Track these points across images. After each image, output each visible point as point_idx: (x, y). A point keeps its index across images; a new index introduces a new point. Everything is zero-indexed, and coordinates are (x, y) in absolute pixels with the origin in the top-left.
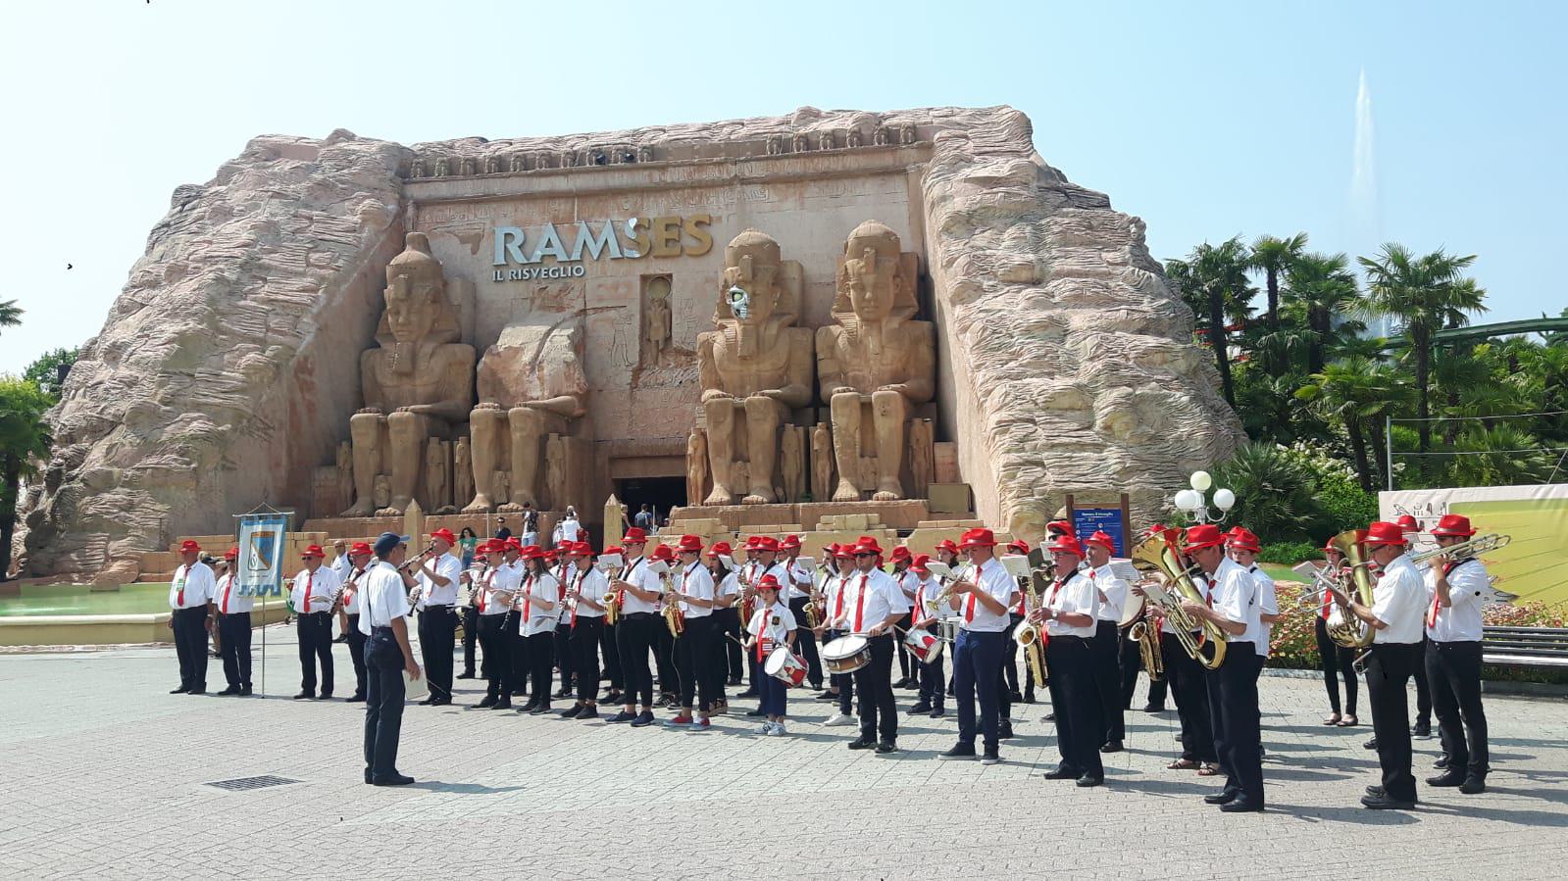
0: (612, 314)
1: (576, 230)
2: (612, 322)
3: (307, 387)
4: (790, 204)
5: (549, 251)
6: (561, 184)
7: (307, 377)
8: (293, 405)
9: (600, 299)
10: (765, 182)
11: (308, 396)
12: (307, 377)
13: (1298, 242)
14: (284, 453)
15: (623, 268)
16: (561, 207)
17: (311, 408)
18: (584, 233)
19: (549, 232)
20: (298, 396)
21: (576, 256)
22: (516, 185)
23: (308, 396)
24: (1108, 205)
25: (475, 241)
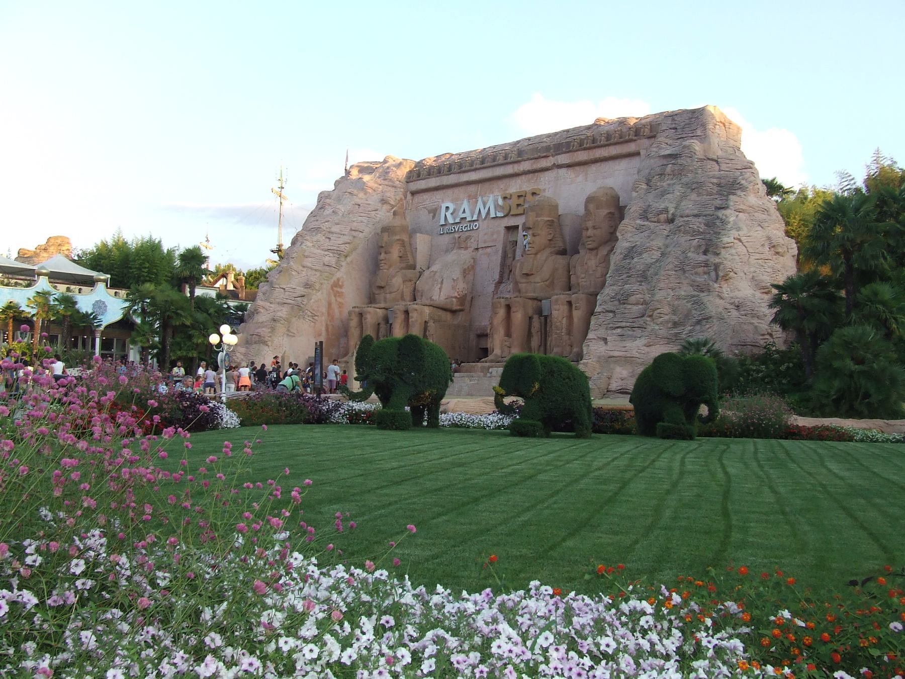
0: (489, 250)
1: (477, 202)
2: (489, 255)
3: (338, 294)
4: (580, 178)
5: (463, 216)
6: (474, 176)
7: (339, 290)
8: (330, 304)
9: (485, 242)
10: (569, 166)
11: (339, 300)
12: (339, 290)
13: (774, 180)
14: (323, 329)
15: (497, 222)
16: (472, 189)
17: (341, 305)
18: (480, 204)
19: (465, 205)
20: (333, 299)
21: (475, 218)
22: (433, 182)
23: (339, 300)
24: (321, 343)
25: (434, 212)
